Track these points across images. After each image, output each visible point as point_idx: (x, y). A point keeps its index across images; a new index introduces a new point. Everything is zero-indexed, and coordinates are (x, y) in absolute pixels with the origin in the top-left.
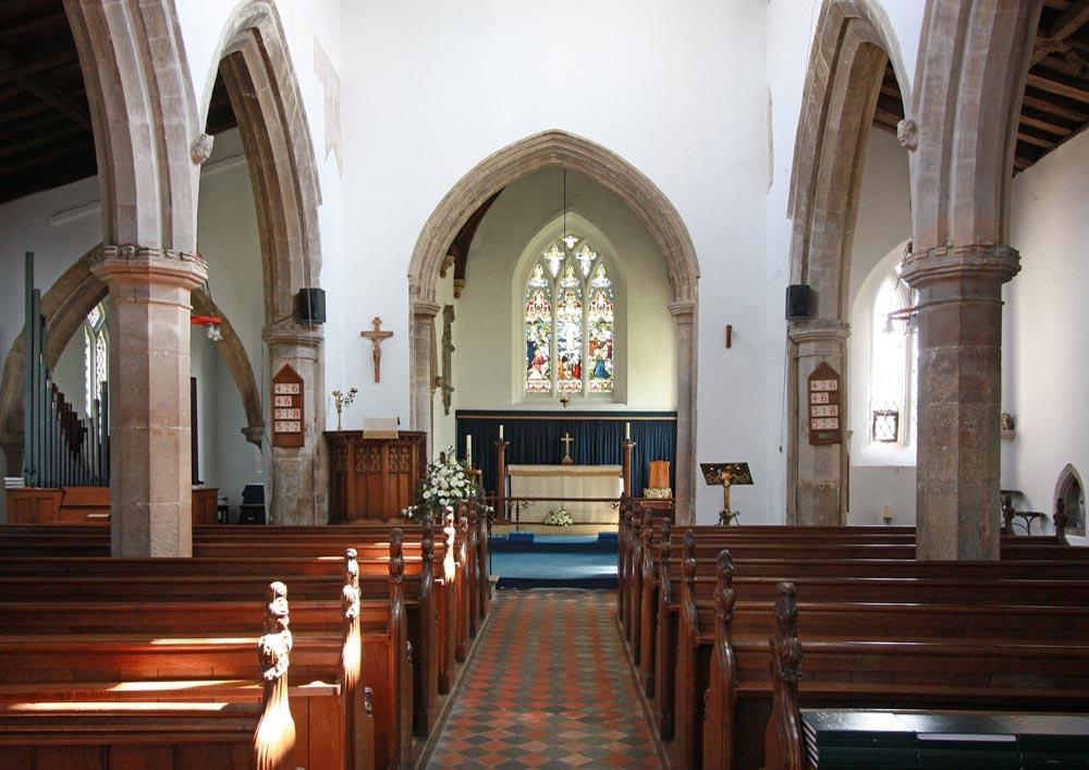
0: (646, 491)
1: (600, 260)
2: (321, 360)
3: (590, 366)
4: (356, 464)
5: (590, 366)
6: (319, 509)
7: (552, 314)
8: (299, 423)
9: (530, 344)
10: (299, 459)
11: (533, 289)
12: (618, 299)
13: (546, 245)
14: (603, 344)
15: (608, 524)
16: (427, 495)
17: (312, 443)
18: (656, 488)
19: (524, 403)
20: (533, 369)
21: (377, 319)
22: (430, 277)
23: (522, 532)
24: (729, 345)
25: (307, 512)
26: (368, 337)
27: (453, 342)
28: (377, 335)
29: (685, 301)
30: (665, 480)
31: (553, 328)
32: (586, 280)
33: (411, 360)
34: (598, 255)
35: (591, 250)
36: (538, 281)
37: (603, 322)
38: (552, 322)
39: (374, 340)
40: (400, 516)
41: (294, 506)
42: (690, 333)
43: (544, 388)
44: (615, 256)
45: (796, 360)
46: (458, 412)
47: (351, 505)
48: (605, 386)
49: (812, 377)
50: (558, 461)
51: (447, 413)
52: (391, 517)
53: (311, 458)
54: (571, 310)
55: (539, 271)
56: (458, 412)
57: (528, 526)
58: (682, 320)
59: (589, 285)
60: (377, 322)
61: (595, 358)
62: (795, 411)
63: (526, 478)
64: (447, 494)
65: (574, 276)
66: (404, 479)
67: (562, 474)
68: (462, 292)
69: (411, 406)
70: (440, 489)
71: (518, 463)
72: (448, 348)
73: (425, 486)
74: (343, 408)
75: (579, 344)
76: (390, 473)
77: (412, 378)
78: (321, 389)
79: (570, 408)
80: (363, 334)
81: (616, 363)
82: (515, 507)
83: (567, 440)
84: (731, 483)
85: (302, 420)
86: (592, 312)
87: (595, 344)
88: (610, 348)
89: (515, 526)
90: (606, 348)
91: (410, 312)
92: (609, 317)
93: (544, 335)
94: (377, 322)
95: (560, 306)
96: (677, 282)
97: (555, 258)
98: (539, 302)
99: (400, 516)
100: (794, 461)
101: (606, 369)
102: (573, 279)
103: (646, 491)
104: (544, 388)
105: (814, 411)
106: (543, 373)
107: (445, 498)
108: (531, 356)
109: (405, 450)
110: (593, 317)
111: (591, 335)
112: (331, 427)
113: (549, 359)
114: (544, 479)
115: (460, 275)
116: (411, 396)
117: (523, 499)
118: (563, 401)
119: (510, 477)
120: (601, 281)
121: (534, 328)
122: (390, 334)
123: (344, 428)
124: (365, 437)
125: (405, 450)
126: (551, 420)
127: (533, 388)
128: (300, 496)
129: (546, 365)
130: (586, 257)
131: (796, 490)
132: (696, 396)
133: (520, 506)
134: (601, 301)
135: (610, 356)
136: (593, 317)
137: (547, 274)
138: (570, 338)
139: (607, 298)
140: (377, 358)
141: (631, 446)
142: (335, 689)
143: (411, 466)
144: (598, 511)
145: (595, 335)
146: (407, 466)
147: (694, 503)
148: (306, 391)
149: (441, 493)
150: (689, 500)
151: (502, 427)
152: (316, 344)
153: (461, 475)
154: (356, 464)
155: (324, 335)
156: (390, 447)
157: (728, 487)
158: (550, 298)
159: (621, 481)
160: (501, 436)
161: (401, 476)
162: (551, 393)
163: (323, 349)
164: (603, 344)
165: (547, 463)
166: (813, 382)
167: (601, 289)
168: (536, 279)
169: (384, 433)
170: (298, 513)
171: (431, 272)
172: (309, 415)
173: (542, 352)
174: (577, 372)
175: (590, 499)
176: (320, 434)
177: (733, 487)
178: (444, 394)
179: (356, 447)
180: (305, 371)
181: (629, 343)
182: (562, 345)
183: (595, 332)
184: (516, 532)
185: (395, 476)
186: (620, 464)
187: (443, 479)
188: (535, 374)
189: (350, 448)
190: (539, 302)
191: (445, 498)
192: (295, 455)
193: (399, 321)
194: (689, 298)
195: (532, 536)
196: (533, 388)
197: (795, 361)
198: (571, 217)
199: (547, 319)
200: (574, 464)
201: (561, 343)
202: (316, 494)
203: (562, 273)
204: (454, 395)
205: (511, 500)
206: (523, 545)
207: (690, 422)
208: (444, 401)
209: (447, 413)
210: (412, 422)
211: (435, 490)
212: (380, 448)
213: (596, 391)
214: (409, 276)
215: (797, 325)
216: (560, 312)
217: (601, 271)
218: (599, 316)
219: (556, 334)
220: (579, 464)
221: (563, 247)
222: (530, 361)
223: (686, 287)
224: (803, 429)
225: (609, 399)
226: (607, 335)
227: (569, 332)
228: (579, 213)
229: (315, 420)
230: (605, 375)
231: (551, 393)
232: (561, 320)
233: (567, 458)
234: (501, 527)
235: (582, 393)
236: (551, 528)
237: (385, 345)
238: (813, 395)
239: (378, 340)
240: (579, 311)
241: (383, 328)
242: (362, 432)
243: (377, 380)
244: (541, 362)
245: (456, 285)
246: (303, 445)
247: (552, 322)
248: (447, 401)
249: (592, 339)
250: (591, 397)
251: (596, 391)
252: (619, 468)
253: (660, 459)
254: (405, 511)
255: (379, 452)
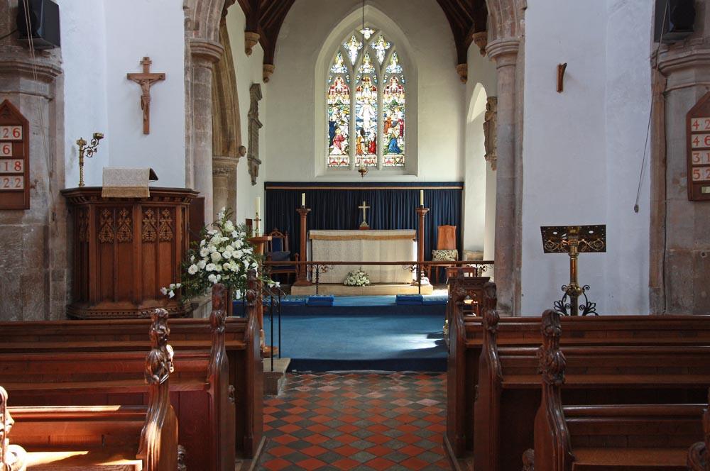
0: (435, 252)
1: (394, 48)
2: (57, 98)
3: (384, 142)
4: (98, 232)
5: (384, 142)
6: (55, 288)
7: (351, 98)
8: (22, 178)
9: (332, 124)
10: (23, 226)
11: (335, 75)
12: (409, 84)
13: (345, 36)
14: (396, 123)
15: (403, 284)
16: (193, 270)
17: (41, 207)
18: (444, 249)
19: (325, 176)
20: (335, 147)
21: (146, 59)
22: (212, 11)
23: (322, 296)
24: (560, 89)
25: (36, 295)
26: (136, 80)
27: (261, 118)
28: (146, 78)
29: (507, 37)
30: (452, 243)
31: (351, 109)
32: (381, 67)
33: (186, 108)
34: (392, 45)
35: (386, 40)
36: (338, 68)
37: (395, 104)
38: (351, 104)
39: (141, 83)
40: (158, 296)
41: (16, 286)
42: (514, 76)
43: (343, 162)
44: (406, 41)
45: (665, 94)
46: (267, 184)
47: (93, 285)
48: (398, 160)
49: (693, 114)
50: (355, 226)
51: (254, 183)
52: (144, 298)
53: (41, 224)
54: (368, 94)
55: (339, 60)
56: (267, 184)
57: (328, 287)
58: (503, 61)
59: (383, 73)
60: (146, 62)
61: (389, 135)
62: (661, 158)
63: (327, 242)
64: (219, 268)
65: (370, 63)
66: (165, 249)
67: (359, 238)
68: (271, 77)
69: (187, 162)
70: (210, 261)
71: (321, 228)
72: (255, 124)
73: (193, 258)
74: (85, 159)
75: (374, 124)
76: (143, 242)
77: (187, 128)
78: (58, 136)
79: (366, 179)
80: (130, 77)
81: (408, 148)
82: (314, 271)
83: (364, 207)
84: (579, 251)
85: (26, 174)
86: (386, 96)
87: (389, 124)
88: (402, 126)
89: (315, 287)
90: (398, 127)
91: (186, 52)
92: (401, 100)
93: (343, 115)
94: (146, 62)
95: (358, 90)
96: (497, 17)
97: (353, 48)
98: (339, 87)
99: (158, 296)
100: (660, 221)
101: (399, 145)
102: (369, 66)
103: (435, 252)
104: (343, 162)
105: (694, 158)
106: (343, 149)
107: (215, 273)
108: (332, 134)
109: (166, 213)
110: (387, 99)
111: (386, 116)
112: (71, 183)
113: (348, 137)
114: (343, 243)
115: (268, 60)
116: (187, 151)
117: (323, 263)
118: (361, 171)
119: (311, 240)
120: (394, 67)
121: (335, 110)
122: (161, 77)
123: (87, 184)
124: (103, 195)
125: (166, 213)
126: (350, 190)
127: (334, 162)
128: (24, 273)
129: (345, 142)
130: (381, 47)
131: (664, 262)
132: (521, 149)
133: (320, 271)
134: (394, 86)
135: (401, 133)
136: (387, 99)
137: (346, 62)
138: (366, 118)
139: (400, 84)
140: (145, 105)
141: (424, 211)
142: (133, 467)
143: (174, 233)
144: (394, 272)
145: (388, 115)
146: (170, 233)
147: (519, 272)
148: (32, 137)
149: (210, 267)
150: (512, 270)
151: (304, 195)
152: (51, 76)
153: (239, 243)
154: (98, 232)
155: (62, 66)
156: (145, 209)
157: (575, 256)
158: (349, 83)
159: (415, 244)
160: (303, 204)
161: (161, 245)
162: (349, 167)
163: (62, 84)
164: (396, 123)
165: (346, 229)
166: (693, 121)
167: (394, 75)
168: (337, 66)
169: (131, 189)
170: (22, 296)
171: (213, 5)
172: (39, 168)
173: (342, 130)
174: (373, 148)
175: (386, 263)
176: (56, 194)
177: (583, 256)
178: (250, 164)
179: (99, 210)
180: (34, 113)
181: (419, 121)
182: (360, 124)
183: (388, 113)
184: (315, 296)
185: (152, 246)
186: (414, 229)
187: (214, 249)
188: (336, 150)
189: (91, 214)
190: (339, 87)
191: (215, 273)
192: (18, 221)
193: (172, 59)
194: (513, 34)
195: (331, 300)
196: (334, 162)
197: (662, 96)
198: (368, 10)
199: (347, 102)
200: (370, 229)
201: (358, 123)
202: (51, 269)
203: (360, 61)
204: (262, 169)
205: (312, 264)
206: (323, 308)
207: (513, 180)
208: (250, 171)
209: (254, 183)
210: (187, 180)
211: (203, 263)
212: (130, 209)
213: (389, 165)
214: (185, 8)
215: (670, 46)
216: (358, 95)
217: (394, 61)
218: (392, 99)
219: (355, 114)
220: (374, 228)
221: (361, 38)
222: (331, 139)
223: (509, 22)
224: (676, 181)
225: (401, 172)
226: (400, 115)
227: (366, 114)
228: (374, 6)
229: (51, 175)
230: (398, 151)
231: (349, 167)
232: (359, 102)
233: (364, 224)
234: (303, 289)
235: (377, 167)
236: (349, 288)
237: (156, 90)
238: (694, 137)
239: (147, 85)
240: (375, 94)
241: (154, 70)
242: (100, 189)
243: (146, 131)
244: (342, 139)
245: (265, 70)
246: (27, 207)
247: (351, 104)
248: (254, 173)
249: (386, 119)
250: (385, 169)
251: (389, 165)
252: (413, 232)
253: (447, 224)
254: (164, 290)
255: (129, 216)
